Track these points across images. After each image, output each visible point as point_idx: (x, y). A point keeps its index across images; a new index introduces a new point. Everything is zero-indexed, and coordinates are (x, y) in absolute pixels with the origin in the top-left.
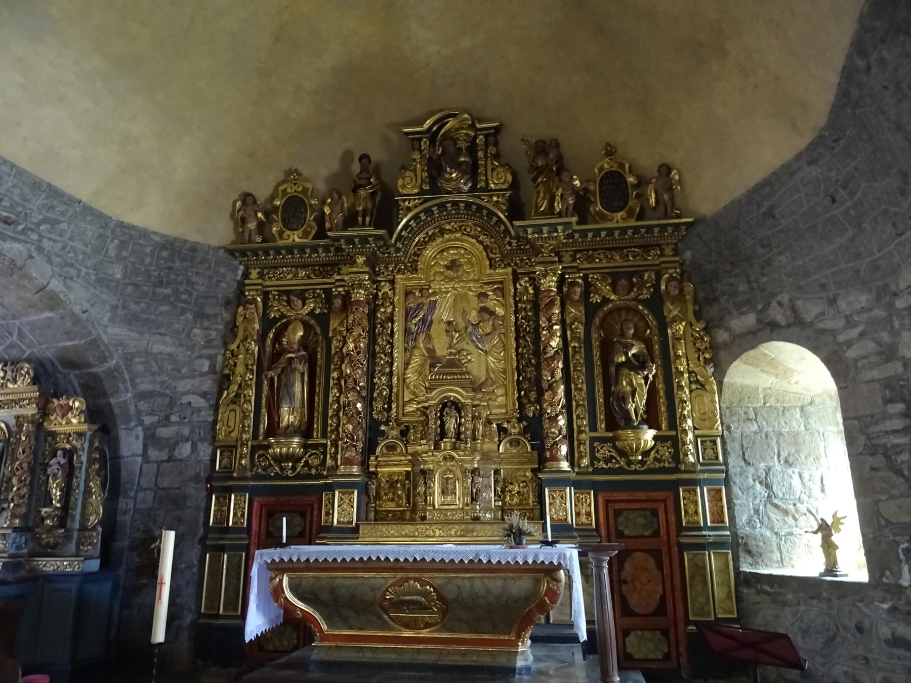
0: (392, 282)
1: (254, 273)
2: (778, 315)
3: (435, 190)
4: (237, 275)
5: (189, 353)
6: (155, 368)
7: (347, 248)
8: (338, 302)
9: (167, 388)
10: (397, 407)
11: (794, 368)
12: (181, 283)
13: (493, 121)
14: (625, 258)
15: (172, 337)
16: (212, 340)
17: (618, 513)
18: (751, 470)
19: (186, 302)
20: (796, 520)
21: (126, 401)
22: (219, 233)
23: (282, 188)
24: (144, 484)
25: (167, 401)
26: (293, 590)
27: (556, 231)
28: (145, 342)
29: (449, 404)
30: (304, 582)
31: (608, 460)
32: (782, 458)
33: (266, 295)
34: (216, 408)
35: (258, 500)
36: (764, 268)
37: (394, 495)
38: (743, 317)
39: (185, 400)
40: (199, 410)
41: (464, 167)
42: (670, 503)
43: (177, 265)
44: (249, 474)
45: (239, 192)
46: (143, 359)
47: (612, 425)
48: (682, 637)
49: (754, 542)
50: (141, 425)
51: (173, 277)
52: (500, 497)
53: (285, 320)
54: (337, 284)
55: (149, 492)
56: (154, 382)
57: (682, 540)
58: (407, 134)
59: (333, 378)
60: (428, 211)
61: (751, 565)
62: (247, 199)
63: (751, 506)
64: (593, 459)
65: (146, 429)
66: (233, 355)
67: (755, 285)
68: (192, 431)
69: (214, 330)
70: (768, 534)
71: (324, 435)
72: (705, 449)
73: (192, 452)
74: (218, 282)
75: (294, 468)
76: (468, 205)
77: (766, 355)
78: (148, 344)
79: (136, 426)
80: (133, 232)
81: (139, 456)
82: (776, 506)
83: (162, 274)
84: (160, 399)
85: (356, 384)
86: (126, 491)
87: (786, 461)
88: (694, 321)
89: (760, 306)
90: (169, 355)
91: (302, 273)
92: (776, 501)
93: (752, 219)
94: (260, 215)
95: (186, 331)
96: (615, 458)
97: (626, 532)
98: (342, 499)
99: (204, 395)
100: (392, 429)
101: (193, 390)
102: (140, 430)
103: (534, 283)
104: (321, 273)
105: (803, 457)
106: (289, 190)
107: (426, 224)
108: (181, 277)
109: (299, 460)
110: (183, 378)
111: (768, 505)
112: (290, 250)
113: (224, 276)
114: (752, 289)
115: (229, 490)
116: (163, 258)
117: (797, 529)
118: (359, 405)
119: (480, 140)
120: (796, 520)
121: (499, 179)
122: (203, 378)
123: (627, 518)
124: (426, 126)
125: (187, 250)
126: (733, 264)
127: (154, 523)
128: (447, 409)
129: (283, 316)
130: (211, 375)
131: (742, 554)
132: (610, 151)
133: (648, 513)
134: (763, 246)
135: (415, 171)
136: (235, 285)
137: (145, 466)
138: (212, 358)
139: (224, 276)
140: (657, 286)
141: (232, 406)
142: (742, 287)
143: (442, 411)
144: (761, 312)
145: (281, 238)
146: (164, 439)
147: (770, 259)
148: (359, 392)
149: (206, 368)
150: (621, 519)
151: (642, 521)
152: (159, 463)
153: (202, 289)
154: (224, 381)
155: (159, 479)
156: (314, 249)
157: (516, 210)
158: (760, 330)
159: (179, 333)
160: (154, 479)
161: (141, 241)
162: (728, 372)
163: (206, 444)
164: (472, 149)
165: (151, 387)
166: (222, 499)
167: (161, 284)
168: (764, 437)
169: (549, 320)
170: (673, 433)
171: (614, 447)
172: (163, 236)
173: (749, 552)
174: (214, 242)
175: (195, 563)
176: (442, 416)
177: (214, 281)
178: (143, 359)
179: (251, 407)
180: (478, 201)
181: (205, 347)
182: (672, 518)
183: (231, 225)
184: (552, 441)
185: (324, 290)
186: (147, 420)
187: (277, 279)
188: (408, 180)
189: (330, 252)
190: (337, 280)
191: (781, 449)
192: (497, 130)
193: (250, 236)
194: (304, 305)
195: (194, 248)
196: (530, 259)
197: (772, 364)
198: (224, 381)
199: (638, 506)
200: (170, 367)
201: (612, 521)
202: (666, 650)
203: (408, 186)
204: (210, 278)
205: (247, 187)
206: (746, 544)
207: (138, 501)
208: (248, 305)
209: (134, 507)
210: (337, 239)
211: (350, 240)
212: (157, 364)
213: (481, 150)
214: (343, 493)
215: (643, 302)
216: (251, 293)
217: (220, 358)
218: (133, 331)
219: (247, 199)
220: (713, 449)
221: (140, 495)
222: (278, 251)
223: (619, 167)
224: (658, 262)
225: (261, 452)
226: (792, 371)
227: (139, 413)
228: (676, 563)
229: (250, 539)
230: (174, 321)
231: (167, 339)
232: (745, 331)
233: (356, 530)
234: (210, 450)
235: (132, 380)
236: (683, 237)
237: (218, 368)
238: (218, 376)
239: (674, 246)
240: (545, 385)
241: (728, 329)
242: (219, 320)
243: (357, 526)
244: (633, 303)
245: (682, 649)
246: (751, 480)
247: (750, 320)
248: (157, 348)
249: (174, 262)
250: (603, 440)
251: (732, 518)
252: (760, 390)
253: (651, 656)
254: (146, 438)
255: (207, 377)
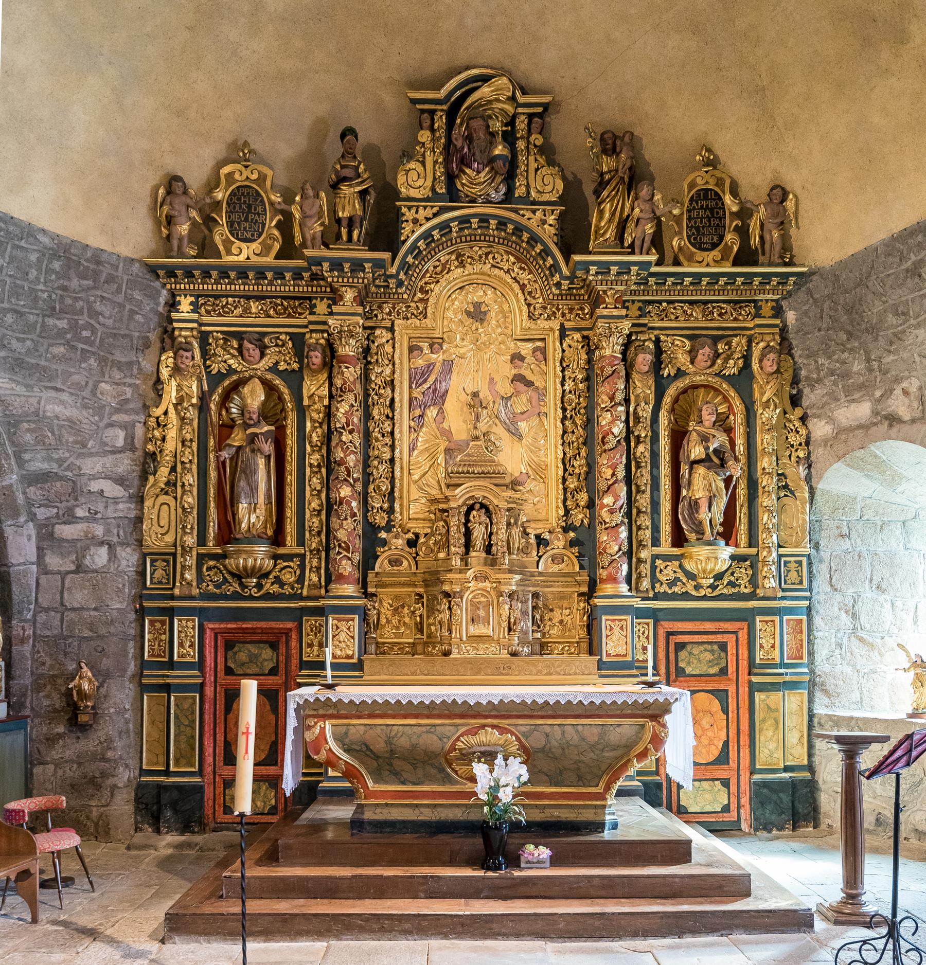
0: (391, 329)
1: (185, 304)
2: (900, 405)
3: (453, 195)
4: (158, 304)
5: (97, 418)
6: (51, 439)
7: (332, 277)
8: (316, 358)
9: (68, 468)
10: (401, 505)
11: (905, 474)
12: (81, 312)
13: (544, 92)
14: (707, 315)
15: (72, 394)
16: (127, 401)
17: (680, 646)
18: (838, 596)
19: (87, 341)
20: (881, 655)
21: (11, 485)
22: (130, 236)
23: (226, 170)
24: (44, 602)
25: (68, 487)
26: (338, 739)
27: (629, 273)
28: (34, 401)
29: (477, 506)
30: (352, 730)
31: (671, 584)
32: (874, 582)
33: (204, 338)
34: (140, 500)
35: (211, 626)
36: (891, 343)
37: (399, 621)
38: (853, 406)
39: (95, 486)
40: (116, 501)
41: (500, 163)
42: (743, 635)
43: (75, 283)
44: (195, 592)
45: (161, 173)
46: (33, 426)
47: (679, 539)
48: (745, 787)
49: (832, 681)
50: (32, 520)
51: (69, 301)
52: (539, 627)
53: (235, 377)
54: (311, 327)
55: (53, 613)
56: (49, 459)
57: (755, 679)
58: (414, 101)
59: (311, 465)
60: (444, 227)
61: (827, 707)
62: (173, 184)
63: (833, 640)
64: (654, 580)
65: (39, 527)
66: (159, 425)
67: (875, 364)
68: (108, 531)
69: (130, 385)
70: (848, 670)
71: (301, 542)
72: (788, 571)
73: (110, 560)
74: (132, 312)
75: (259, 586)
76: (502, 223)
77: (876, 456)
78: (39, 403)
79: (27, 521)
80: (11, 228)
81: (33, 564)
82: (861, 640)
83: (54, 296)
84: (58, 484)
85: (349, 475)
86: (20, 612)
87: (878, 587)
88: (788, 407)
89: (878, 394)
90: (69, 420)
91: (254, 307)
92: (861, 634)
93: (888, 276)
94: (194, 214)
95: (91, 384)
96: (681, 581)
97: (689, 670)
98: (338, 628)
99: (120, 481)
100: (396, 537)
101: (102, 474)
102: (31, 529)
103: (588, 345)
104: (285, 309)
105: (898, 582)
106: (237, 176)
107: (441, 246)
108: (81, 303)
109: (266, 575)
110: (91, 455)
111: (853, 639)
112: (242, 272)
113: (139, 304)
114: (871, 370)
115: (171, 613)
116: (53, 271)
117: (882, 666)
118: (354, 504)
119: (521, 124)
120: (881, 655)
121: (545, 184)
122: (118, 456)
123: (690, 653)
124: (443, 92)
125: (87, 260)
126: (850, 335)
127: (66, 654)
128: (474, 513)
129: (231, 371)
130: (128, 453)
131: (818, 694)
132: (712, 163)
133: (715, 647)
134: (897, 314)
135: (423, 163)
136: (156, 319)
137: (43, 580)
138: (128, 427)
139: (139, 304)
140: (747, 358)
141: (163, 498)
142: (857, 366)
143: (468, 514)
144: (878, 401)
145: (229, 252)
146: (67, 541)
147: (903, 332)
148: (353, 486)
149: (120, 442)
150: (683, 654)
151: (708, 656)
152: (64, 575)
153: (110, 322)
154: (149, 462)
155: (66, 595)
156: (279, 274)
157: (573, 237)
158: (875, 424)
159: (82, 389)
160: (58, 597)
161: (23, 243)
162: (825, 476)
163: (128, 550)
164: (510, 138)
165: (45, 466)
166: (158, 625)
167: (52, 312)
168: (856, 557)
169: (612, 398)
170: (753, 551)
171: (681, 566)
172: (54, 237)
173: (826, 692)
174: (126, 251)
175: (127, 707)
176: (468, 521)
177: (126, 313)
178: (33, 426)
179: (191, 500)
180: (513, 216)
181: (117, 411)
182: (744, 653)
183: (149, 224)
184: (609, 559)
185: (292, 336)
186: (42, 513)
187: (220, 315)
188: (413, 175)
189: (302, 278)
190: (311, 323)
191: (875, 572)
192: (546, 107)
193: (180, 247)
194: (263, 355)
195: (98, 257)
196: (582, 309)
197: (880, 466)
198: (149, 462)
199: (704, 638)
200: (71, 439)
201: (672, 656)
202: (726, 802)
203: (416, 180)
204: (121, 306)
205: (174, 165)
206: (823, 684)
207: (38, 625)
208: (181, 352)
209: (34, 633)
210: (318, 262)
211: (336, 265)
212: (53, 434)
213: (522, 137)
214: (339, 620)
215: (729, 379)
216: (183, 333)
217: (139, 430)
218: (17, 383)
219: (173, 184)
220: (797, 571)
221: (42, 617)
222: (224, 273)
223: (717, 185)
224: (751, 325)
225: (212, 563)
226: (901, 477)
227: (30, 503)
228: (744, 705)
229: (204, 676)
230: (73, 370)
231: (65, 396)
232: (854, 424)
233: (359, 666)
234: (134, 558)
235: (18, 456)
236: (790, 293)
237: (138, 443)
238: (139, 453)
239: (774, 304)
240: (603, 486)
241: (831, 420)
242: (135, 371)
243: (360, 661)
244: (717, 379)
245: (745, 800)
246: (836, 609)
247: (863, 410)
248: (52, 409)
249: (69, 279)
250: (667, 558)
251: (811, 653)
252: (858, 499)
253: (708, 809)
254: (40, 538)
255: (122, 455)
